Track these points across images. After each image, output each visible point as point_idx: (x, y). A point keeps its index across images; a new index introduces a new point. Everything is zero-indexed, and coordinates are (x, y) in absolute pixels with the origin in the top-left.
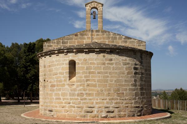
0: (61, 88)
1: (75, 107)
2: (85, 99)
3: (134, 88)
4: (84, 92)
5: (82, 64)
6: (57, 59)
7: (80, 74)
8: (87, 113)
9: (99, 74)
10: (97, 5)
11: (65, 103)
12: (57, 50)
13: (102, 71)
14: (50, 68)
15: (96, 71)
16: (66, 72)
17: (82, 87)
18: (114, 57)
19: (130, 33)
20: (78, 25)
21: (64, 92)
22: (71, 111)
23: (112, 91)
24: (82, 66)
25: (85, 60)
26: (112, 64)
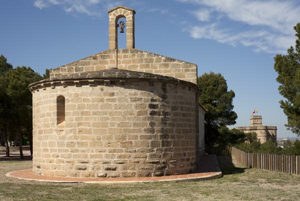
1: (64, 162)
2: (77, 151)
3: (149, 134)
4: (75, 141)
6: (44, 95)
9: (95, 115)
10: (125, 12)
11: (53, 156)
13: (100, 110)
15: (91, 111)
18: (116, 89)
20: (197, 33)
21: (52, 140)
23: (114, 138)
25: (77, 95)
26: (113, 100)
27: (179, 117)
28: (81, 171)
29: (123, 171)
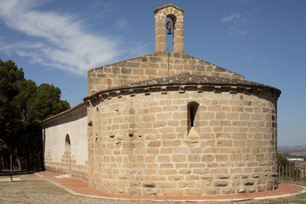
0: (173, 147)
2: (216, 165)
4: (213, 154)
6: (165, 99)
7: (207, 125)
10: (176, 12)
11: (181, 172)
12: (166, 85)
13: (239, 120)
14: (146, 114)
16: (181, 122)
17: (209, 147)
18: (253, 98)
19: (60, 57)
21: (178, 154)
22: (192, 185)
24: (210, 112)
26: (250, 110)
28: (220, 188)
29: (258, 185)
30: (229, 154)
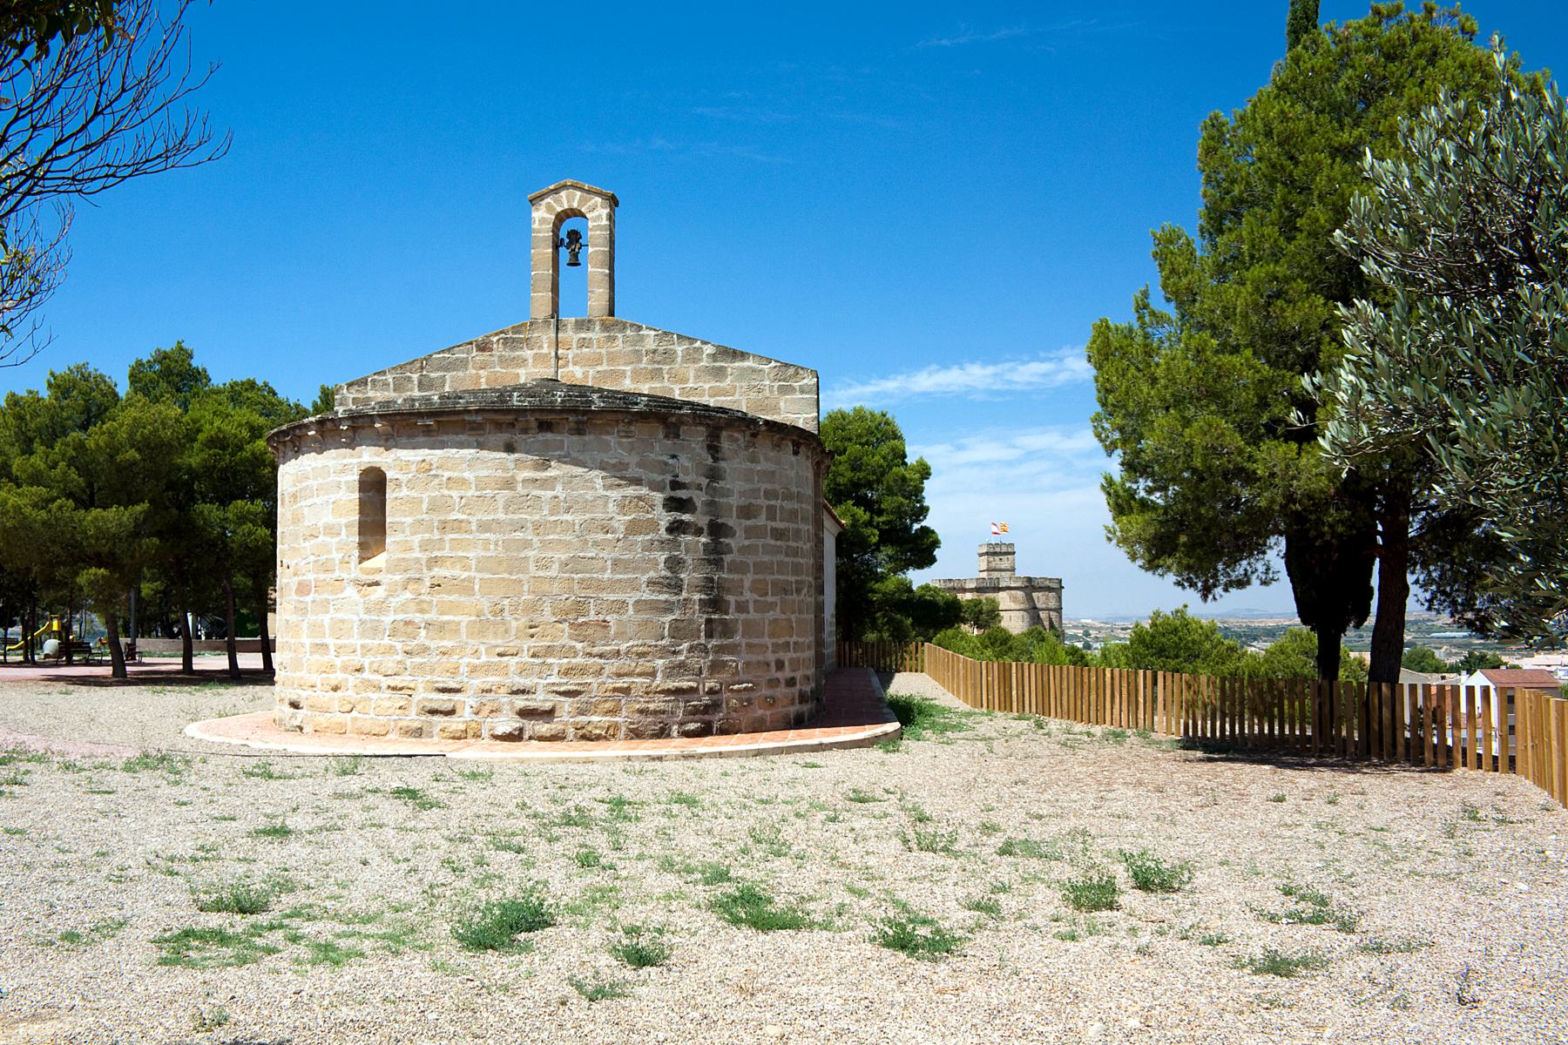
2: (425, 650)
4: (418, 618)
5: (411, 484)
8: (430, 717)
13: (501, 516)
17: (408, 595)
21: (339, 616)
23: (547, 610)
24: (413, 493)
27: (760, 542)
28: (436, 718)
30: (465, 619)
